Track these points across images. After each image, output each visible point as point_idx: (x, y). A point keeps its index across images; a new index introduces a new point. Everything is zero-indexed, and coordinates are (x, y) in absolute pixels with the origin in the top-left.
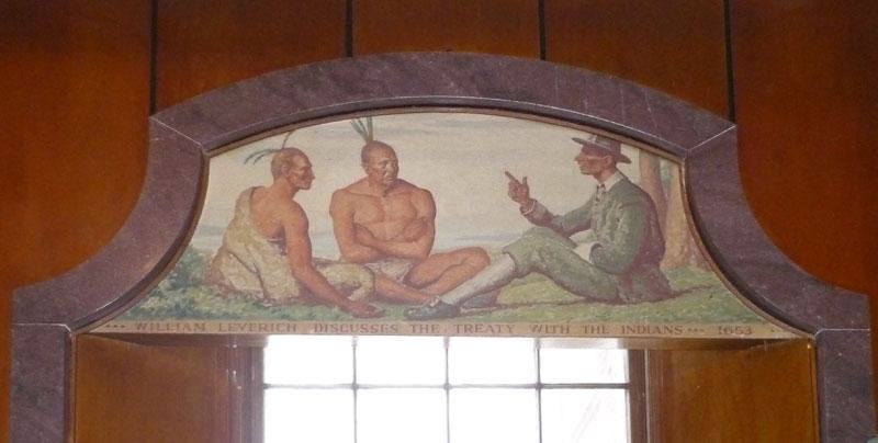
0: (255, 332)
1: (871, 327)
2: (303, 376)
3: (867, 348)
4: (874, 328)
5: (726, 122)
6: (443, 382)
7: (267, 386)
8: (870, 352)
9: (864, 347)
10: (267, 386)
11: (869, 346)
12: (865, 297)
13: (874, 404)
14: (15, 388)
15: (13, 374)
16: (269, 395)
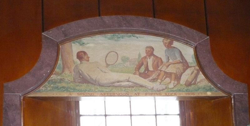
0: (74, 95)
1: (248, 93)
2: (89, 106)
3: (247, 99)
4: (249, 93)
5: (205, 36)
6: (132, 117)
7: (178, 115)
8: (248, 100)
9: (246, 99)
10: (178, 115)
11: (247, 99)
12: (246, 84)
13: (249, 115)
14: (4, 110)
15: (4, 106)
16: (178, 112)
